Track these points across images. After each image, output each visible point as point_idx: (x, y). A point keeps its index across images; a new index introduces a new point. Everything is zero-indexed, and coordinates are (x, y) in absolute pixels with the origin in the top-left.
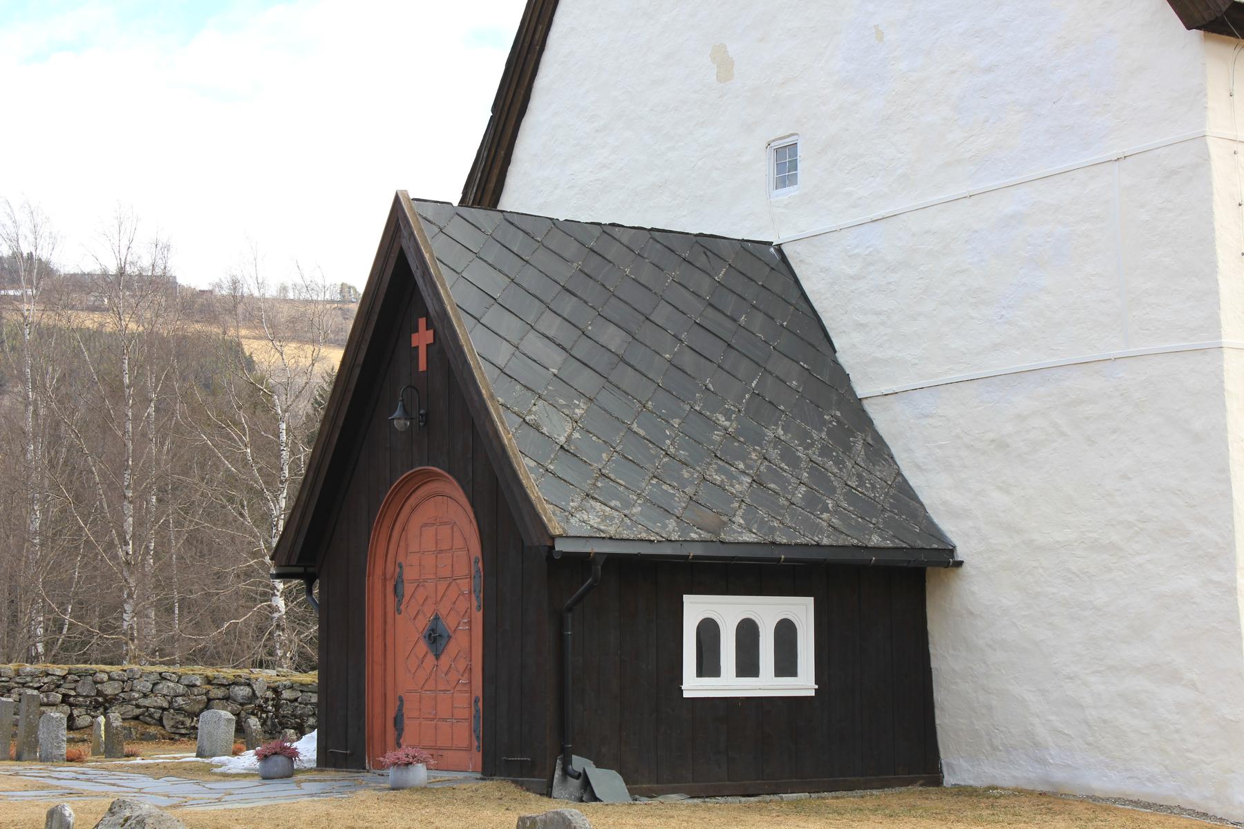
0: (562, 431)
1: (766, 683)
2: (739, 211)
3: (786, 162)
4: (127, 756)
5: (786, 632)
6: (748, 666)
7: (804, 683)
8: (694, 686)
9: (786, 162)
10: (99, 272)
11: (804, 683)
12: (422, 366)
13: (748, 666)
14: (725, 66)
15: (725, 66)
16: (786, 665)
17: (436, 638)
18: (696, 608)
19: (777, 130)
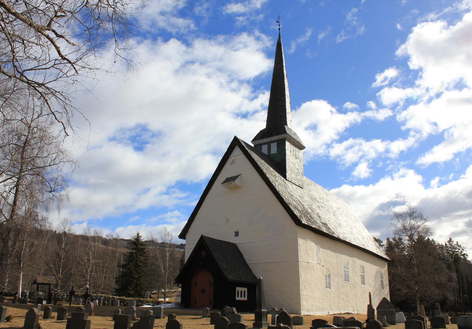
0: (225, 267)
1: (243, 299)
2: (232, 239)
3: (237, 234)
4: (52, 318)
5: (245, 292)
6: (241, 297)
7: (246, 299)
8: (237, 298)
9: (237, 234)
10: (160, 241)
11: (246, 299)
12: (203, 256)
13: (241, 297)
14: (228, 220)
15: (228, 220)
16: (244, 297)
17: (203, 291)
18: (238, 289)
19: (236, 229)
